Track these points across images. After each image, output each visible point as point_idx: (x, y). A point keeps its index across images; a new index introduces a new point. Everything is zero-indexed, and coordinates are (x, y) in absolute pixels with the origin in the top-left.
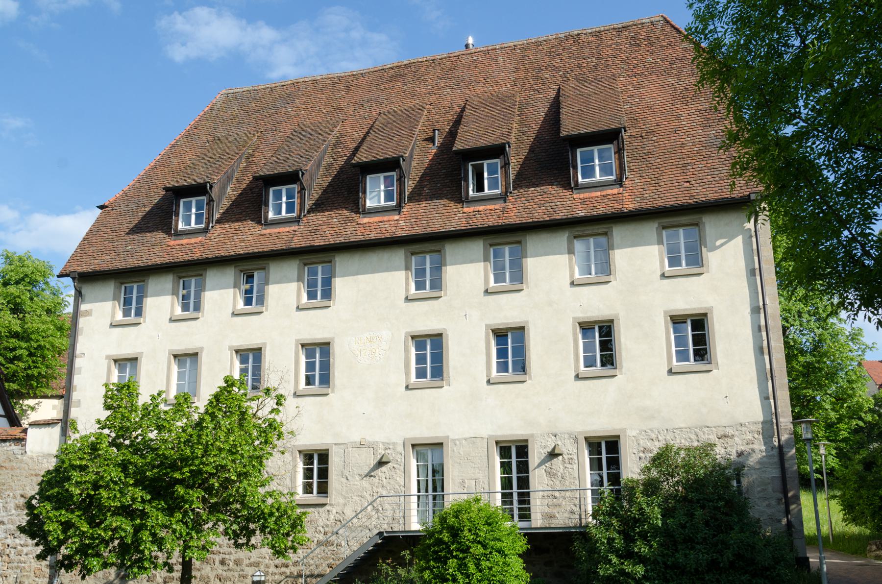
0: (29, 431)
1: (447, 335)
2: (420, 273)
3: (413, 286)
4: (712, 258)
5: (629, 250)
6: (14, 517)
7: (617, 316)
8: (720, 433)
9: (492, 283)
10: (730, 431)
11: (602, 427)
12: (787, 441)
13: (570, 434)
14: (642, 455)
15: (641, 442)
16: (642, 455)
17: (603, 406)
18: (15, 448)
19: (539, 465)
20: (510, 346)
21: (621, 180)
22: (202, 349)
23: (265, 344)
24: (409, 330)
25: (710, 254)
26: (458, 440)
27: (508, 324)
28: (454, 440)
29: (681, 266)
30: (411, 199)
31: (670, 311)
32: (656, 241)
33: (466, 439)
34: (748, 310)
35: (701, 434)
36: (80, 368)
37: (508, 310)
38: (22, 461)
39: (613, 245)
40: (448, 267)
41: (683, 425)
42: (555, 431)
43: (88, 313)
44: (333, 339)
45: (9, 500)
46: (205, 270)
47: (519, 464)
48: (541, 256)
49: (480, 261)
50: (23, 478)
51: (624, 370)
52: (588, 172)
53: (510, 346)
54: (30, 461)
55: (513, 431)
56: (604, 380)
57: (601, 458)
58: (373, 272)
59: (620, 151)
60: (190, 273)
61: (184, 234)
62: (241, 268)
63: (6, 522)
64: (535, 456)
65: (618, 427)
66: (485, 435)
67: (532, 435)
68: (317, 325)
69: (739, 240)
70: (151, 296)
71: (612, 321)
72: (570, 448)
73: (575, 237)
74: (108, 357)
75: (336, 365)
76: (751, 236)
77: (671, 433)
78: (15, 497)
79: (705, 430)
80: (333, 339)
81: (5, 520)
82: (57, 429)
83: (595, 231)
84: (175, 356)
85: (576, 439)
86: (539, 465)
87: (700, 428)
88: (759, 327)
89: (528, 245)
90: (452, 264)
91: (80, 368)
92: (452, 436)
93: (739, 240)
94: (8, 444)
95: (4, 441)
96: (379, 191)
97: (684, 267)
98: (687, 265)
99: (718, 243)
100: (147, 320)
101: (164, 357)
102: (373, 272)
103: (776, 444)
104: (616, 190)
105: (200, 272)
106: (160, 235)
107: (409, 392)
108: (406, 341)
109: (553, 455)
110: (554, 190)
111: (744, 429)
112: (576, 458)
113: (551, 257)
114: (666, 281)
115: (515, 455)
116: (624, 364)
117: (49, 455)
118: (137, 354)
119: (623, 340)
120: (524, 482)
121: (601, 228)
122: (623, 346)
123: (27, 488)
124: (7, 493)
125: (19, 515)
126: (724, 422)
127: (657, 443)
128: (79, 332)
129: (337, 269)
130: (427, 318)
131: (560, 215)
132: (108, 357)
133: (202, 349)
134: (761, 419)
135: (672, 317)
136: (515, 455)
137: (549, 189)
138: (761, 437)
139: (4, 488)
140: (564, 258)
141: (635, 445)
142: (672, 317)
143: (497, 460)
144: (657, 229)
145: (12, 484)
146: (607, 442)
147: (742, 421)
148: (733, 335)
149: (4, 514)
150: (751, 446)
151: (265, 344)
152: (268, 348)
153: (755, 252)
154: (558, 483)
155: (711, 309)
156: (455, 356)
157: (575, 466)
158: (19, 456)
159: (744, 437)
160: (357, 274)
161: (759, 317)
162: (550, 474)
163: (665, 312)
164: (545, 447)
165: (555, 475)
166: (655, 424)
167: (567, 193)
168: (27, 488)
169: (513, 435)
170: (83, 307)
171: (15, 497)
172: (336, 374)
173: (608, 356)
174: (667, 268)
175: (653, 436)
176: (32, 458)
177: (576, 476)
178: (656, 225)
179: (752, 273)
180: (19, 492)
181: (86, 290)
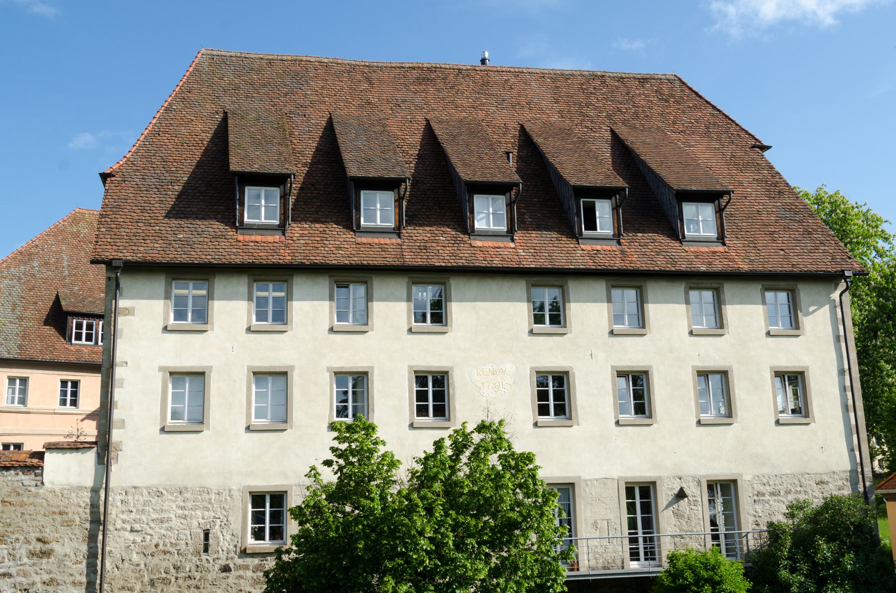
0: (47, 456)
1: (574, 374)
2: (261, 303)
3: (172, 315)
4: (806, 321)
5: (738, 307)
6: (27, 568)
7: (731, 367)
8: (818, 480)
9: (171, 320)
10: (825, 478)
11: (721, 471)
12: (870, 486)
13: (694, 478)
14: (756, 498)
15: (755, 486)
16: (756, 498)
17: (637, 453)
18: (27, 479)
19: (667, 507)
20: (638, 389)
21: (284, 226)
22: (292, 368)
23: (372, 368)
24: (535, 365)
25: (805, 319)
26: (590, 480)
27: (632, 367)
28: (585, 481)
29: (186, 320)
30: (409, 223)
31: (776, 367)
32: (163, 294)
33: (597, 480)
34: (836, 372)
35: (803, 480)
36: (122, 380)
37: (634, 353)
38: (36, 495)
39: (372, 297)
40: (572, 304)
41: (789, 472)
42: (680, 474)
43: (129, 312)
44: (452, 368)
45: (17, 545)
46: (292, 276)
47: (272, 514)
48: (661, 303)
49: (403, 301)
50: (40, 517)
51: (739, 419)
52: (256, 214)
53: (638, 389)
54: (50, 496)
55: (641, 472)
56: (722, 428)
57: (634, 503)
58: (493, 300)
59: (719, 211)
60: (271, 277)
61: (251, 228)
62: (337, 278)
63: (15, 574)
64: (664, 496)
65: (734, 472)
66: (615, 476)
67: (660, 478)
68: (432, 351)
69: (827, 308)
70: (377, 301)
71: (447, 373)
72: (694, 490)
73: (413, 283)
74: (161, 369)
75: (457, 397)
76: (836, 307)
77: (779, 479)
78: (27, 542)
79: (806, 476)
80: (452, 368)
81: (13, 571)
82: (90, 457)
83: (708, 285)
84: (255, 373)
85: (699, 483)
86: (667, 507)
87: (802, 475)
88: (845, 387)
89: (649, 290)
90: (461, 301)
91: (122, 380)
92: (585, 476)
93: (827, 308)
94: (12, 472)
95: (7, 468)
96: (488, 214)
97: (188, 323)
98: (192, 320)
99: (811, 309)
100: (215, 327)
101: (242, 377)
102: (493, 300)
103: (861, 489)
104: (277, 237)
105: (284, 278)
106: (217, 227)
107: (538, 430)
108: (248, 377)
109: (681, 495)
110: (335, 230)
111: (836, 476)
112: (700, 500)
113: (671, 305)
114: (770, 339)
115: (641, 497)
116: (739, 414)
117: (80, 488)
118: (287, 367)
119: (736, 391)
120: (648, 524)
121: (714, 283)
122: (737, 397)
123: (47, 530)
124: (14, 536)
125: (34, 564)
126: (821, 470)
127: (768, 488)
128: (118, 334)
129: (453, 293)
130: (552, 353)
131: (683, 267)
132: (328, 369)
133: (292, 368)
134: (849, 468)
135: (698, 372)
136: (641, 497)
137: (656, 236)
138: (849, 484)
139: (10, 529)
140: (681, 308)
141: (750, 489)
142: (698, 372)
143: (624, 501)
144: (685, 288)
145: (24, 525)
146: (640, 488)
147: (835, 470)
148: (829, 391)
149: (11, 563)
150: (842, 492)
151: (372, 368)
152: (376, 373)
153: (840, 321)
154: (684, 523)
155: (410, 367)
156: (660, 393)
157: (700, 508)
158: (33, 489)
159: (836, 483)
160: (475, 300)
161: (844, 378)
162: (678, 515)
163: (771, 368)
164: (672, 489)
165: (682, 516)
166: (766, 470)
167: (231, 233)
168: (47, 530)
169: (641, 477)
170: (122, 303)
171: (27, 542)
172: (457, 406)
173: (642, 405)
174: (254, 322)
175: (765, 481)
176: (53, 491)
177: (701, 517)
178: (760, 287)
179: (837, 339)
180: (33, 536)
181: (126, 282)
